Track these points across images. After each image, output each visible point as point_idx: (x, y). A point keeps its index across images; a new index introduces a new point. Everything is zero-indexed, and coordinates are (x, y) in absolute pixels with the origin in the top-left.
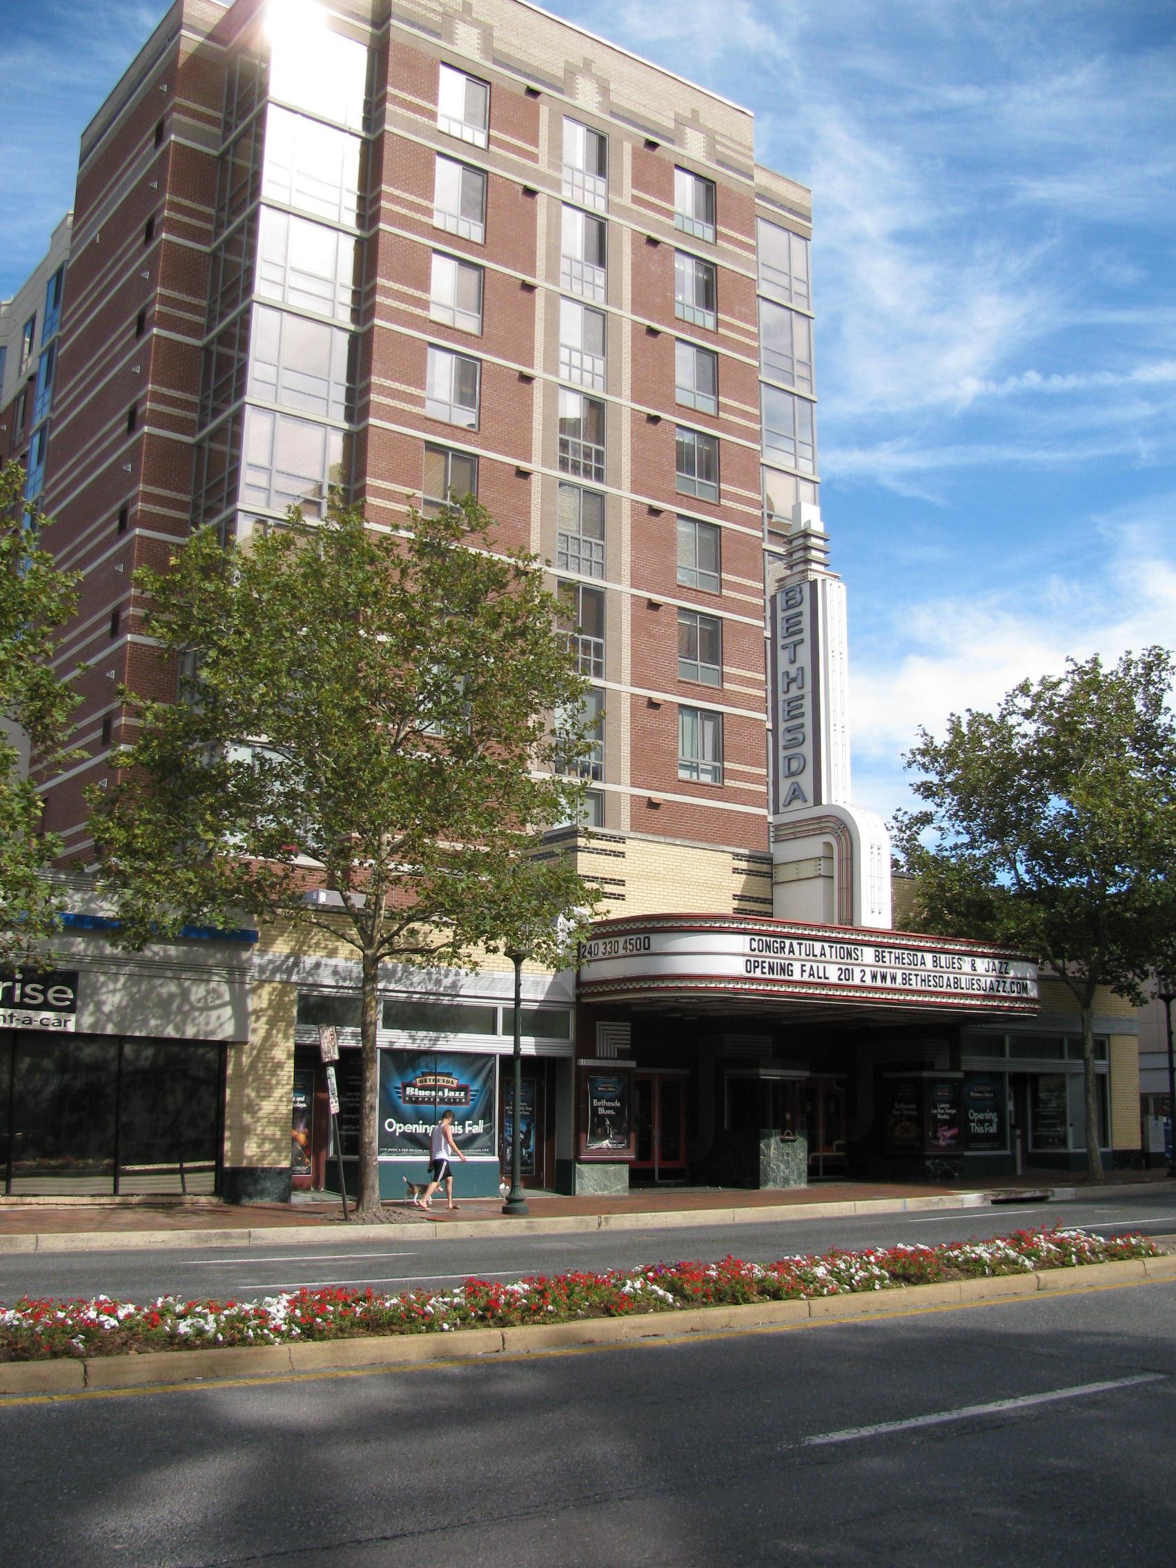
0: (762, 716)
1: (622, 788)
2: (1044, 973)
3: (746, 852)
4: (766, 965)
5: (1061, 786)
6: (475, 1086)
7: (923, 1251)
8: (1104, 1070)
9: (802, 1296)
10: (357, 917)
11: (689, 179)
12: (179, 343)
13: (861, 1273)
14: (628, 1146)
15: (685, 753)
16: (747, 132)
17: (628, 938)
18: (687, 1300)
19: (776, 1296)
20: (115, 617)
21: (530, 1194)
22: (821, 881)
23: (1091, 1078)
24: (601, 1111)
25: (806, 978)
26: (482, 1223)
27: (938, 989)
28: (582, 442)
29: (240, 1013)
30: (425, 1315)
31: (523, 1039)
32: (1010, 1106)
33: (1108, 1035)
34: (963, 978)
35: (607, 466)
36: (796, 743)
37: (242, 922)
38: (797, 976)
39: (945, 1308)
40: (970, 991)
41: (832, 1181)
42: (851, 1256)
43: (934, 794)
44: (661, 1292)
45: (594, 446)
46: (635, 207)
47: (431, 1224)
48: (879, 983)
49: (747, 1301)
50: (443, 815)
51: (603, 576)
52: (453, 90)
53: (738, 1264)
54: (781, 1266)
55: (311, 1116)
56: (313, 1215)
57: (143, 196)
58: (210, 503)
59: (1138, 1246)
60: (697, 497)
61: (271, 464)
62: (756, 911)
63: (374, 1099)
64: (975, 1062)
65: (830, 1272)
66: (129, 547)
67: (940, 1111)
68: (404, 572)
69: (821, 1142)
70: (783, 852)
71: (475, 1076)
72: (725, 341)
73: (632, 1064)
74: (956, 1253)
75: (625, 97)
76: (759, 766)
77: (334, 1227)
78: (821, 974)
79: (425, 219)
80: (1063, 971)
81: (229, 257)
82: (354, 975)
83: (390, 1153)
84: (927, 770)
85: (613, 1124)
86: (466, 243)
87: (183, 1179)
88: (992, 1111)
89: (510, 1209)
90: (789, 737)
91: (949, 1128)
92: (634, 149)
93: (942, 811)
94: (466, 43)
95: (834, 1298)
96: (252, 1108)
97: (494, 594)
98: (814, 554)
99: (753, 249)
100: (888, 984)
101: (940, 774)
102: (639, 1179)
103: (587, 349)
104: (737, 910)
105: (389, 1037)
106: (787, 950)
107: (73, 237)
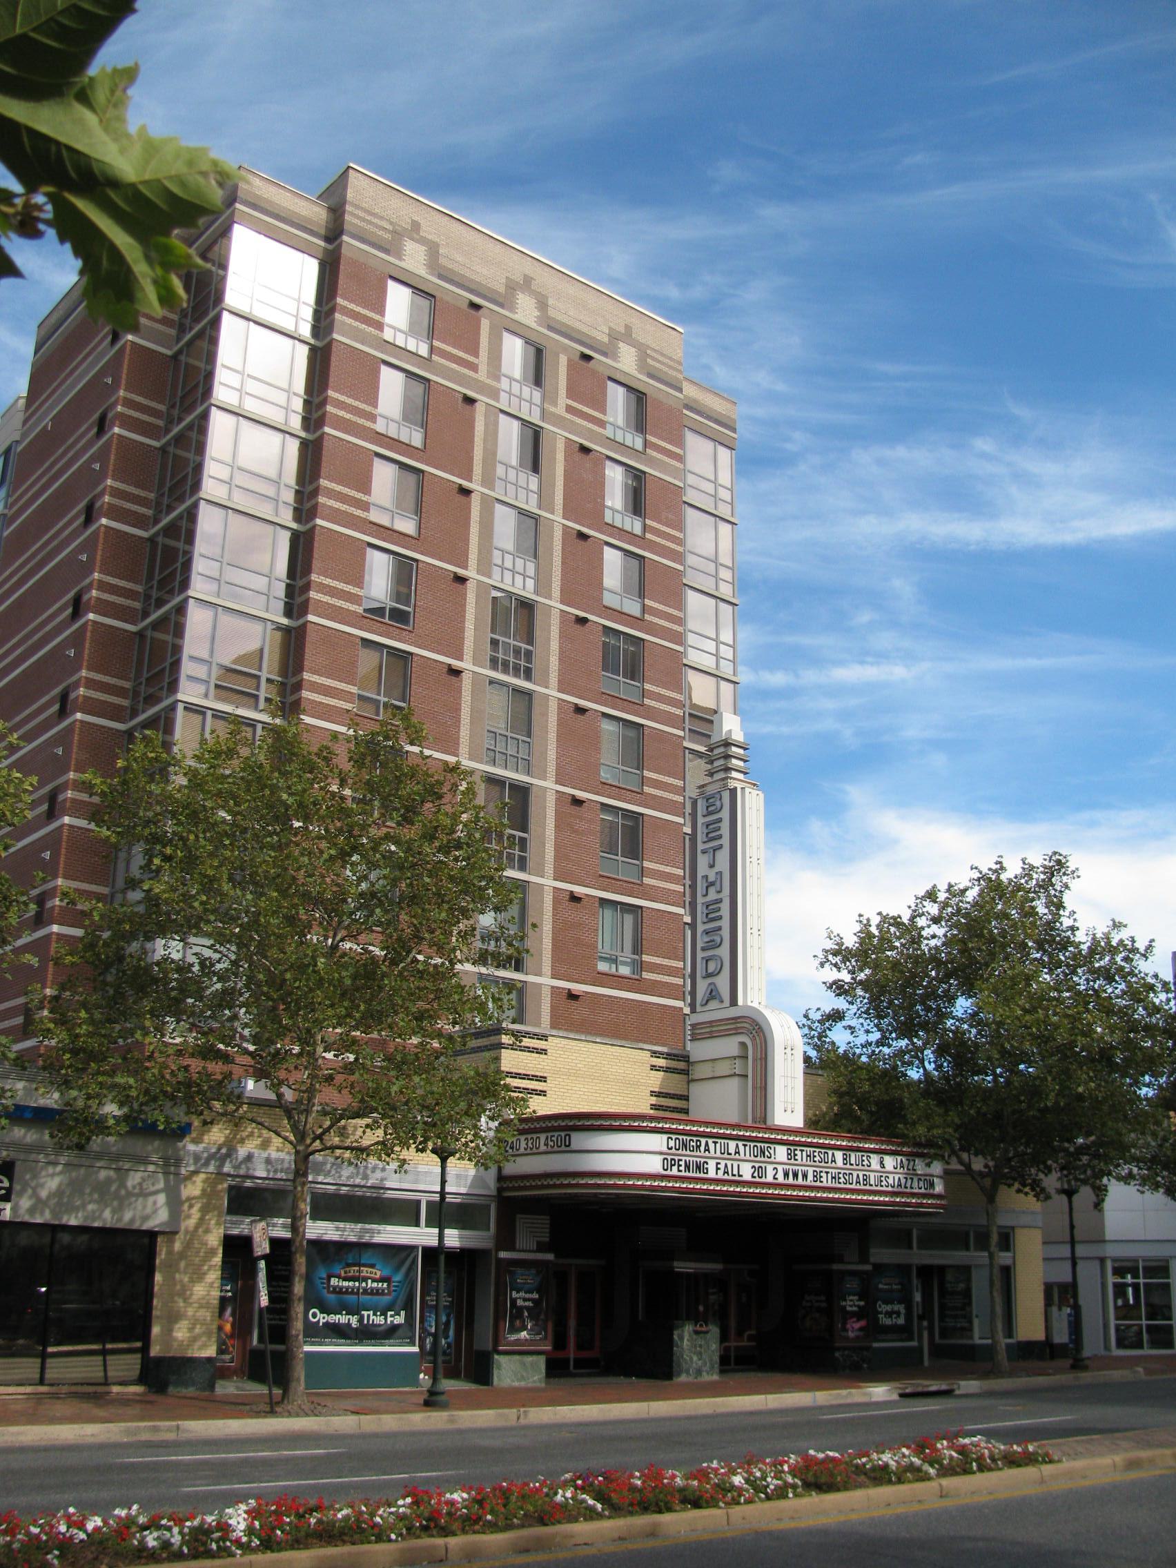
0: (680, 911)
1: (542, 979)
3: (665, 1050)
4: (682, 1163)
6: (398, 1278)
7: (834, 1459)
8: (1009, 1262)
11: (621, 391)
12: (126, 533)
13: (775, 1482)
14: (546, 1338)
15: (605, 943)
16: (672, 341)
17: (549, 1134)
18: (616, 1509)
19: (696, 1504)
20: (52, 798)
21: (448, 1385)
23: (996, 1271)
24: (520, 1303)
25: (720, 1175)
27: (848, 1186)
28: (511, 641)
29: (175, 1203)
30: (375, 1526)
31: (447, 1231)
32: (918, 1297)
33: (1013, 1228)
35: (536, 665)
37: (179, 1114)
38: (712, 1174)
39: (854, 1516)
40: (879, 1188)
41: (742, 1371)
44: (591, 1502)
45: (524, 646)
46: (568, 416)
47: (355, 1418)
48: (791, 1180)
49: (669, 1509)
52: (398, 300)
54: (702, 1475)
55: (237, 1300)
57: (97, 391)
58: (151, 690)
59: (1035, 1453)
61: (211, 656)
62: (672, 1111)
63: (298, 1288)
64: (882, 1255)
65: (747, 1481)
66: (70, 729)
71: (397, 1269)
72: (652, 546)
73: (550, 1257)
74: (864, 1460)
75: (563, 312)
76: (676, 958)
77: (260, 1420)
78: (735, 1172)
79: (368, 424)
80: (968, 1167)
81: (180, 452)
82: (286, 1165)
83: (313, 1344)
84: (839, 969)
85: (530, 1316)
86: (406, 448)
87: (105, 1361)
88: (900, 1303)
89: (432, 1401)
91: (858, 1320)
92: (569, 361)
93: (854, 1008)
94: (414, 259)
95: (750, 1506)
96: (184, 1294)
97: (431, 805)
99: (680, 458)
100: (800, 1181)
101: (852, 972)
102: (556, 1368)
103: (519, 550)
104: (654, 1107)
105: (317, 1229)
106: (702, 1148)
107: (25, 422)
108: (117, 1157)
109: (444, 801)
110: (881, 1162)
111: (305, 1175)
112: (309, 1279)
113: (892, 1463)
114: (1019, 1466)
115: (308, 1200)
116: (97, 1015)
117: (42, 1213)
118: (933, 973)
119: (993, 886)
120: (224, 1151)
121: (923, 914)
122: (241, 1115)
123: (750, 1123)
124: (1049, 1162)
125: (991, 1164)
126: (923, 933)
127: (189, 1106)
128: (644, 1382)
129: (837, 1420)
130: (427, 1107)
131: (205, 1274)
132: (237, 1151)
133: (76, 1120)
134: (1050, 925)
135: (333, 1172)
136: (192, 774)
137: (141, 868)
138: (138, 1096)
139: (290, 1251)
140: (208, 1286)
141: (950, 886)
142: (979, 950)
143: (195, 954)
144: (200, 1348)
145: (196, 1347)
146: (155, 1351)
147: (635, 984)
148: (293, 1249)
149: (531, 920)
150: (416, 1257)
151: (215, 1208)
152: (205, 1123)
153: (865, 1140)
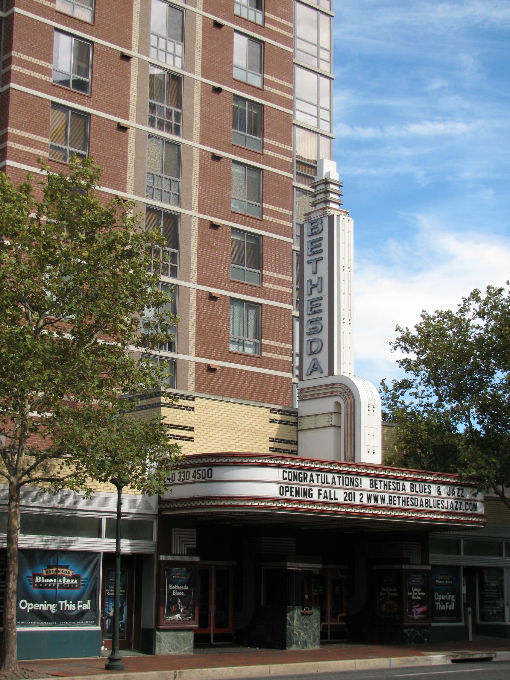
1: (189, 357)
3: (280, 407)
4: (294, 490)
6: (85, 575)
14: (194, 618)
17: (197, 469)
21: (123, 654)
22: (332, 430)
24: (175, 593)
25: (321, 499)
27: (414, 507)
28: (165, 106)
31: (122, 541)
32: (464, 590)
34: (432, 499)
35: (183, 124)
36: (316, 331)
38: (315, 498)
40: (437, 509)
45: (174, 109)
48: (372, 503)
51: (178, 204)
60: (247, 148)
62: (285, 452)
64: (438, 558)
67: (414, 593)
73: (197, 559)
78: (332, 497)
85: (183, 603)
90: (311, 326)
91: (420, 607)
100: (379, 503)
102: (201, 641)
104: (272, 449)
106: (308, 479)
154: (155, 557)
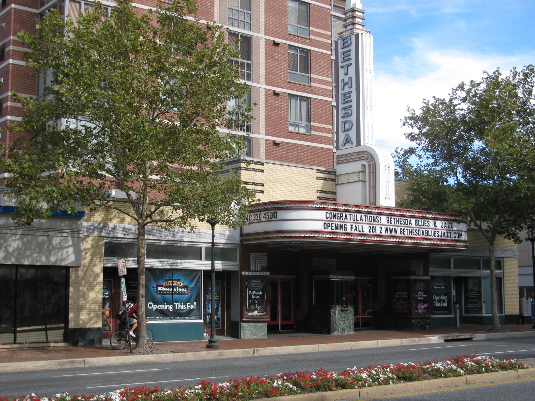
0: (330, 99)
1: (260, 136)
2: (470, 227)
3: (324, 169)
5: (480, 135)
6: (192, 286)
7: (412, 366)
8: (501, 275)
9: (356, 387)
10: (133, 204)
13: (383, 376)
14: (267, 314)
15: (292, 119)
17: (266, 212)
18: (303, 390)
19: (344, 387)
22: (360, 183)
23: (494, 280)
24: (253, 297)
25: (353, 231)
26: (197, 353)
27: (418, 236)
29: (76, 252)
31: (216, 262)
32: (454, 293)
33: (503, 258)
34: (430, 230)
37: (78, 207)
38: (349, 230)
39: (423, 393)
40: (434, 237)
42: (378, 368)
43: (416, 139)
44: (291, 386)
47: (173, 354)
48: (389, 234)
49: (330, 389)
50: (175, 154)
53: (326, 372)
54: (346, 373)
55: (112, 299)
56: (113, 350)
62: (327, 200)
63: (142, 291)
64: (435, 271)
65: (369, 376)
66: (9, 13)
68: (155, 33)
69: (360, 310)
70: (341, 169)
71: (192, 281)
73: (268, 274)
74: (427, 366)
76: (328, 124)
77: (126, 357)
78: (361, 229)
80: (480, 227)
82: (133, 231)
84: (413, 127)
89: (210, 345)
90: (344, 112)
91: (423, 304)
95: (371, 388)
96: (84, 296)
97: (201, 45)
98: (357, 20)
100: (393, 234)
102: (272, 329)
104: (318, 198)
106: (344, 218)
108: (47, 230)
109: (207, 42)
110: (435, 224)
111: (143, 235)
112: (147, 287)
113: (441, 367)
114: (507, 370)
115: (145, 248)
116: (34, 157)
117: (10, 259)
118: (462, 128)
119: (494, 82)
120: (102, 225)
121: (456, 98)
122: (108, 205)
123: (368, 205)
124: (522, 225)
125: (491, 226)
126: (457, 108)
127: (83, 202)
128: (316, 335)
129: (413, 351)
130: (203, 197)
131: (95, 286)
132: (108, 225)
133: (25, 210)
134: (524, 103)
135: (157, 234)
136: (77, 33)
137: (52, 82)
138: (57, 197)
139: (137, 274)
140: (97, 292)
141: (472, 82)
142: (486, 115)
143: (83, 126)
144: (94, 324)
145: (91, 323)
146: (71, 325)
147: (308, 137)
148: (139, 272)
149: (254, 101)
150: (200, 278)
151: (98, 253)
152: (91, 210)
153: (427, 213)
154: (239, 272)
